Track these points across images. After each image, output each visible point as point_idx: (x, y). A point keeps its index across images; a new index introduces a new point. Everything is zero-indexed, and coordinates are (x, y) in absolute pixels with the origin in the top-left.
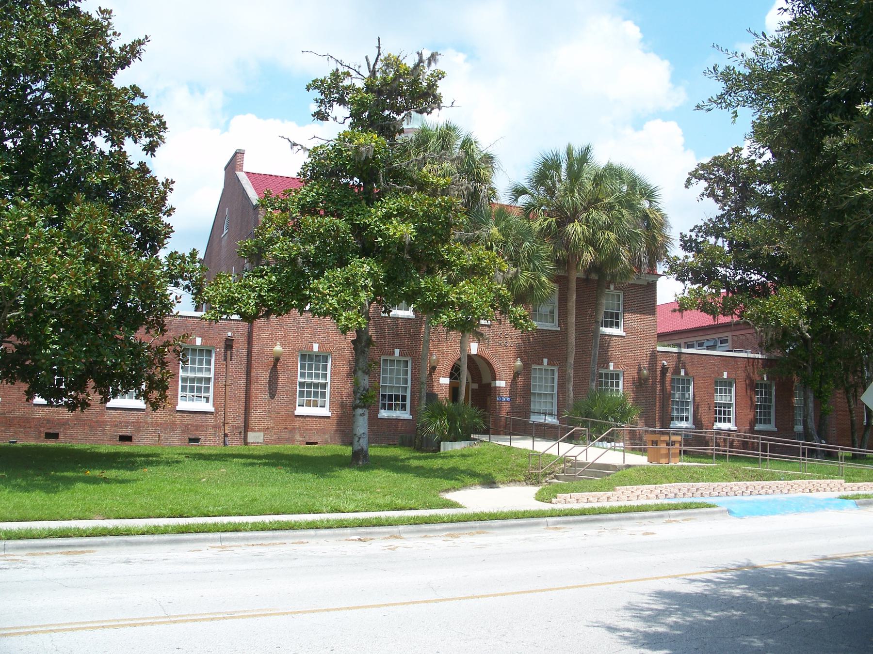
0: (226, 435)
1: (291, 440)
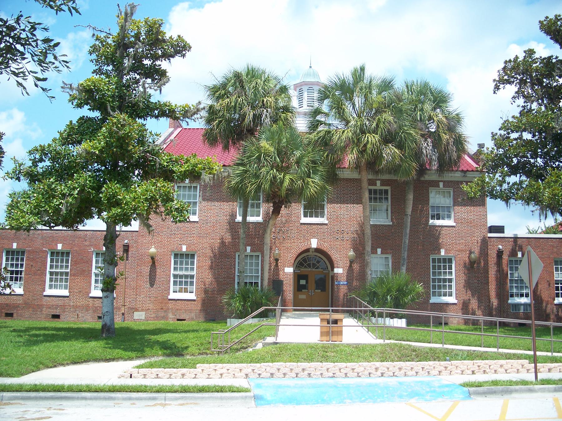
0: (123, 314)
1: (165, 318)
